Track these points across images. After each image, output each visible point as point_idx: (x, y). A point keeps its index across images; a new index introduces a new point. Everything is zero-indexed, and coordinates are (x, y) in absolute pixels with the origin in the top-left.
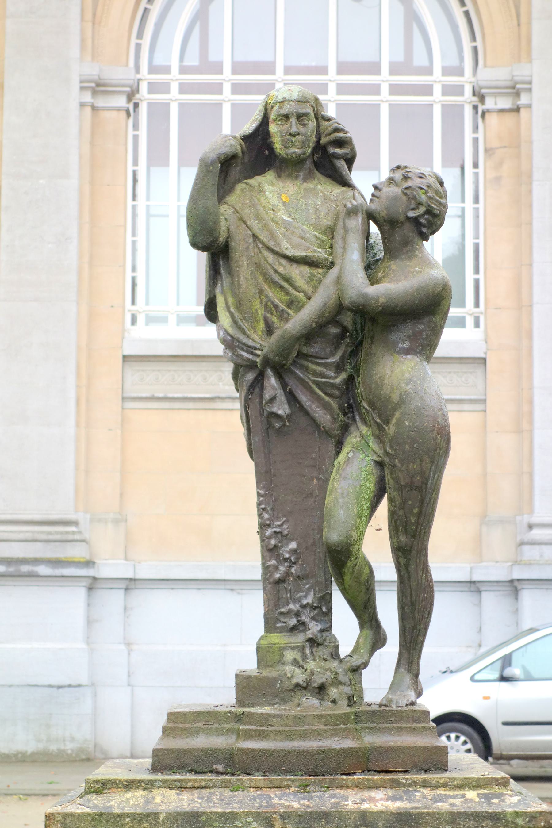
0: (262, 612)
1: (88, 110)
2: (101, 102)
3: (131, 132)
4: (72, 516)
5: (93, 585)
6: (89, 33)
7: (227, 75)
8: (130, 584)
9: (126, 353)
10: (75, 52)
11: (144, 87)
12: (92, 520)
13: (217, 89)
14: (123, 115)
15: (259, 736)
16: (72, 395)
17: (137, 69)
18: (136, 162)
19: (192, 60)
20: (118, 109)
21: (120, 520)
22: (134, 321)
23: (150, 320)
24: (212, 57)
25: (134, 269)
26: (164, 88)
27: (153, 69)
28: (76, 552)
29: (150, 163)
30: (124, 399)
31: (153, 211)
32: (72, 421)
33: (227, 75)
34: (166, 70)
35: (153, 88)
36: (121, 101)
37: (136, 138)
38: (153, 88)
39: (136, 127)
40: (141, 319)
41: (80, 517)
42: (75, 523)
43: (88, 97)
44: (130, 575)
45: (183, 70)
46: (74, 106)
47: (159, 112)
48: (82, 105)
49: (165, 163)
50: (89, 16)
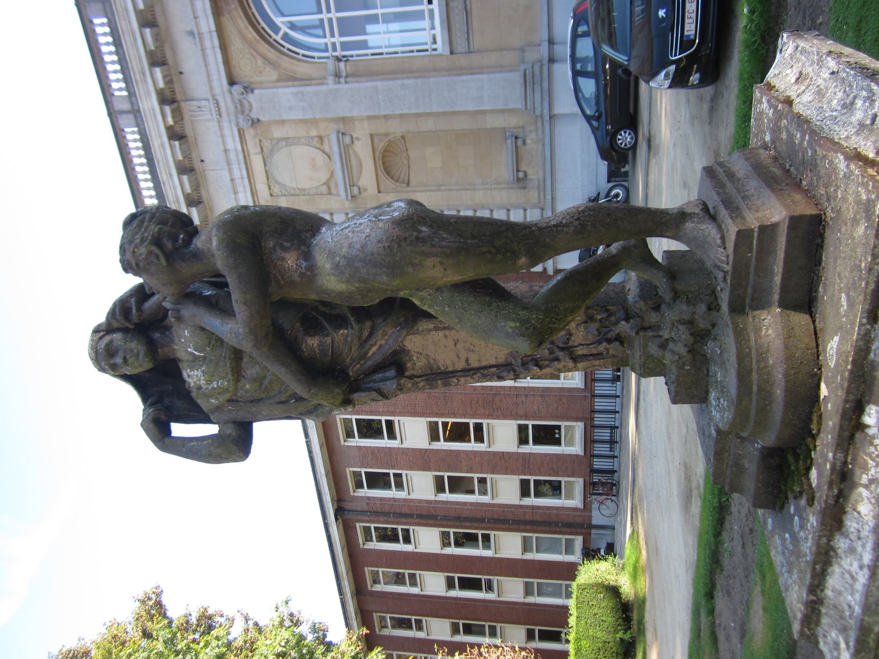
0: (253, 446)
1: (348, 79)
2: (344, 74)
3: (355, 58)
4: (522, 72)
5: (551, 60)
6: (315, 82)
7: (324, 16)
8: (551, 42)
9: (448, 53)
10: (324, 87)
11: (335, 54)
12: (523, 63)
13: (330, 20)
14: (348, 63)
15: (612, 442)
16: (469, 77)
17: (328, 58)
18: (367, 55)
19: (319, 32)
20: (345, 66)
21: (522, 50)
22: (435, 50)
23: (435, 42)
24: (318, 23)
25: (412, 51)
26: (334, 44)
27: (326, 50)
28: (537, 69)
29: (368, 48)
30: (470, 52)
31: (387, 44)
32: (481, 76)
33: (324, 16)
34: (326, 44)
35: (335, 50)
36: (342, 64)
37: (357, 56)
38: (335, 50)
39: (352, 56)
40: (434, 46)
41: (522, 68)
42: (525, 70)
43: (342, 80)
44: (546, 43)
45: (325, 37)
46: (347, 86)
47: (345, 46)
48: (346, 82)
49: (365, 42)
50: (308, 82)
